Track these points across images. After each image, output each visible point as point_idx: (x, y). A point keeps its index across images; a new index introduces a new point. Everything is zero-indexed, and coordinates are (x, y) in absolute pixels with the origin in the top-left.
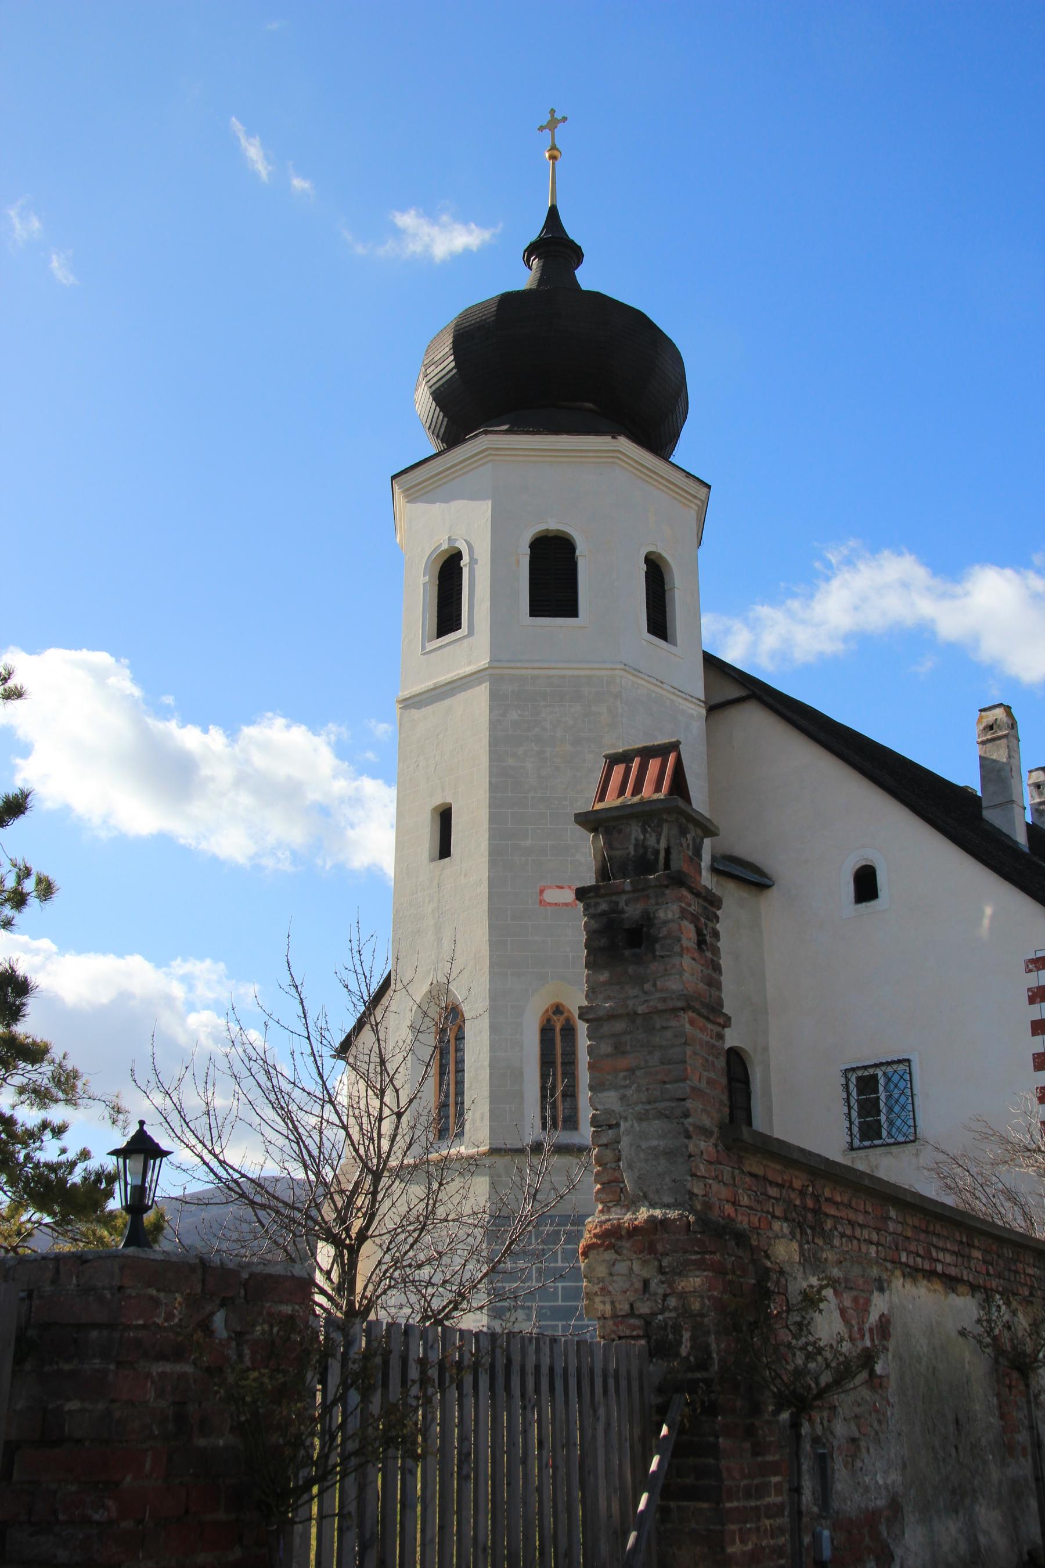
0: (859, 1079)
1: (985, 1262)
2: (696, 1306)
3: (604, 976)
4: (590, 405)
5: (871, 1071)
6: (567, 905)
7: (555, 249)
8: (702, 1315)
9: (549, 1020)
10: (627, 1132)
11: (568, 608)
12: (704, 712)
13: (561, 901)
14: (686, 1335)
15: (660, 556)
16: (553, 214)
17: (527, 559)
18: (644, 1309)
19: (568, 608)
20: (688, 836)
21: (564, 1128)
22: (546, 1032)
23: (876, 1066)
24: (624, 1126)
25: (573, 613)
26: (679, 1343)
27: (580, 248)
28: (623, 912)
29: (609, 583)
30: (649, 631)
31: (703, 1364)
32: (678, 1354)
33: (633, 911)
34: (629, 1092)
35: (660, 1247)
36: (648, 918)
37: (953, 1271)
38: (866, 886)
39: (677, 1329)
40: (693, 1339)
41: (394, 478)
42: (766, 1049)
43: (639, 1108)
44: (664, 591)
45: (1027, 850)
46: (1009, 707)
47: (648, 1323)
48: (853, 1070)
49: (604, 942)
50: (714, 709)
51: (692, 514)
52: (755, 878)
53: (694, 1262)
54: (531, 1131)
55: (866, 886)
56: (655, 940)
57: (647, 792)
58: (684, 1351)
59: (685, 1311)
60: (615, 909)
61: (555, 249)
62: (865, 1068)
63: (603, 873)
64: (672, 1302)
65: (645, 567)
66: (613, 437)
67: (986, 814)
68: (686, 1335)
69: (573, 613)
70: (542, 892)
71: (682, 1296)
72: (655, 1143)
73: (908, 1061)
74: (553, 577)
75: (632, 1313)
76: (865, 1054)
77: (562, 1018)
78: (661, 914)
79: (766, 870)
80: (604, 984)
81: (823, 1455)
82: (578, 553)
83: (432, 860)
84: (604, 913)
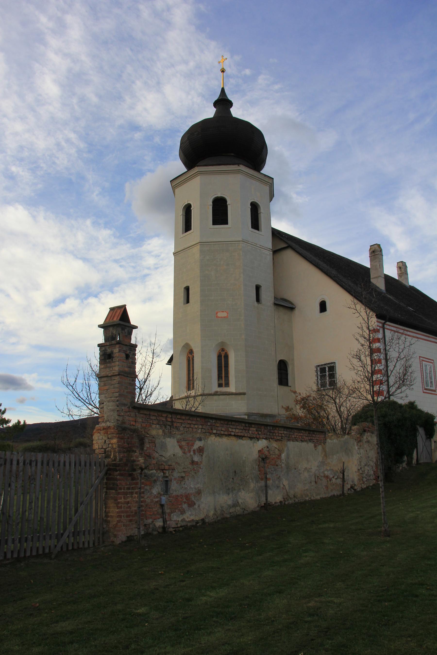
0: (320, 368)
1: (257, 431)
2: (115, 446)
3: (103, 367)
4: (233, 154)
5: (324, 366)
6: (225, 317)
7: (223, 103)
8: (115, 449)
9: (220, 353)
10: (106, 405)
11: (225, 222)
12: (272, 253)
13: (223, 316)
14: (112, 453)
15: (256, 202)
16: (223, 90)
17: (211, 207)
18: (104, 447)
19: (225, 222)
20: (126, 330)
21: (225, 387)
22: (219, 357)
23: (325, 364)
24: (105, 403)
25: (226, 223)
26: (111, 455)
27: (231, 101)
28: (107, 350)
29: (238, 213)
30: (252, 227)
31: (115, 460)
32: (110, 457)
33: (109, 351)
34: (106, 395)
35: (109, 433)
36: (112, 352)
37: (239, 434)
38: (323, 307)
39: (111, 452)
40: (114, 454)
41: (171, 181)
42: (293, 360)
43: (108, 399)
44: (258, 214)
45: (385, 292)
46: (380, 245)
47: (105, 450)
48: (318, 366)
49: (103, 358)
50: (275, 252)
51: (267, 188)
52: (290, 306)
53: (115, 436)
54: (215, 388)
55: (323, 307)
56: (113, 357)
57: (115, 319)
58: (112, 457)
59: (112, 448)
60: (106, 350)
61: (223, 103)
62: (322, 365)
63: (106, 339)
64: (110, 445)
65: (250, 207)
66: (238, 165)
67: (372, 280)
68: (112, 453)
69: (226, 223)
70: (217, 313)
71: (112, 444)
72: (110, 408)
73: (335, 363)
74: (220, 211)
75: (102, 448)
76: (323, 361)
77: (224, 352)
78: (115, 351)
79: (293, 303)
80: (103, 368)
81: (167, 481)
82: (228, 204)
83: (184, 304)
84: (103, 351)
